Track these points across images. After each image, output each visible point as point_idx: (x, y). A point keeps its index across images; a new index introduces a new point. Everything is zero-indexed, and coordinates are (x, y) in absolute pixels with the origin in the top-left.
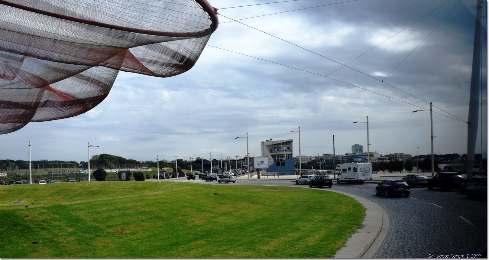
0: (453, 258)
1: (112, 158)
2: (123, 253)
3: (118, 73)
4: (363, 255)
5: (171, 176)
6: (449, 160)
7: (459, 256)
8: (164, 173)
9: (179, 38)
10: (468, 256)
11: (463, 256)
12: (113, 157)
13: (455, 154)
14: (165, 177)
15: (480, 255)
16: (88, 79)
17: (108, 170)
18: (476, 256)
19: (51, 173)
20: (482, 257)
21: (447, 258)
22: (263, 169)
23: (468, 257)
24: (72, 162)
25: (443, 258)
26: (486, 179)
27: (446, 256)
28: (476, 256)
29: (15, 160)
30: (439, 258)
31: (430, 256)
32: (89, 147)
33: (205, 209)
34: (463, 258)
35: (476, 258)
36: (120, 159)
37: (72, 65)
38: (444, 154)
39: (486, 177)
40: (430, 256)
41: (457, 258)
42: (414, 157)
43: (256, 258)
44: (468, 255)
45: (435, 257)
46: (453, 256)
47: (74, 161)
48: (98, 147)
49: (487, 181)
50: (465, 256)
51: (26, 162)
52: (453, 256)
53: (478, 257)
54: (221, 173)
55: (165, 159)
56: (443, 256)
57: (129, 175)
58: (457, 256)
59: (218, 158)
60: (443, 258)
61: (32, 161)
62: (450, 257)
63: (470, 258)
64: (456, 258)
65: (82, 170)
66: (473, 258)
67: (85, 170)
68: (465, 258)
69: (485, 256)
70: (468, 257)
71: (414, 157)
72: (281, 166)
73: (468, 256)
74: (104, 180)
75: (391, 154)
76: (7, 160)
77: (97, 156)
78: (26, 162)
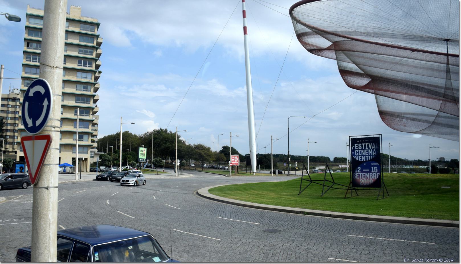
0: (432, 262)
1: (384, 156)
6: (33, 103)
7: (433, 260)
10: (441, 260)
11: (437, 260)
12: (385, 156)
15: (452, 260)
16: (128, 33)
20: (454, 262)
24: (343, 158)
32: (308, 142)
33: (410, 191)
34: (436, 262)
37: (453, 116)
41: (431, 262)
44: (441, 259)
45: (411, 261)
46: (427, 260)
48: (277, 139)
49: (459, 178)
51: (280, 155)
52: (427, 260)
53: (451, 262)
55: (406, 159)
58: (431, 260)
60: (417, 262)
63: (443, 262)
65: (405, 166)
67: (407, 166)
68: (439, 262)
69: (458, 261)
70: (441, 261)
72: (309, 156)
73: (441, 260)
74: (256, 170)
78: (280, 155)
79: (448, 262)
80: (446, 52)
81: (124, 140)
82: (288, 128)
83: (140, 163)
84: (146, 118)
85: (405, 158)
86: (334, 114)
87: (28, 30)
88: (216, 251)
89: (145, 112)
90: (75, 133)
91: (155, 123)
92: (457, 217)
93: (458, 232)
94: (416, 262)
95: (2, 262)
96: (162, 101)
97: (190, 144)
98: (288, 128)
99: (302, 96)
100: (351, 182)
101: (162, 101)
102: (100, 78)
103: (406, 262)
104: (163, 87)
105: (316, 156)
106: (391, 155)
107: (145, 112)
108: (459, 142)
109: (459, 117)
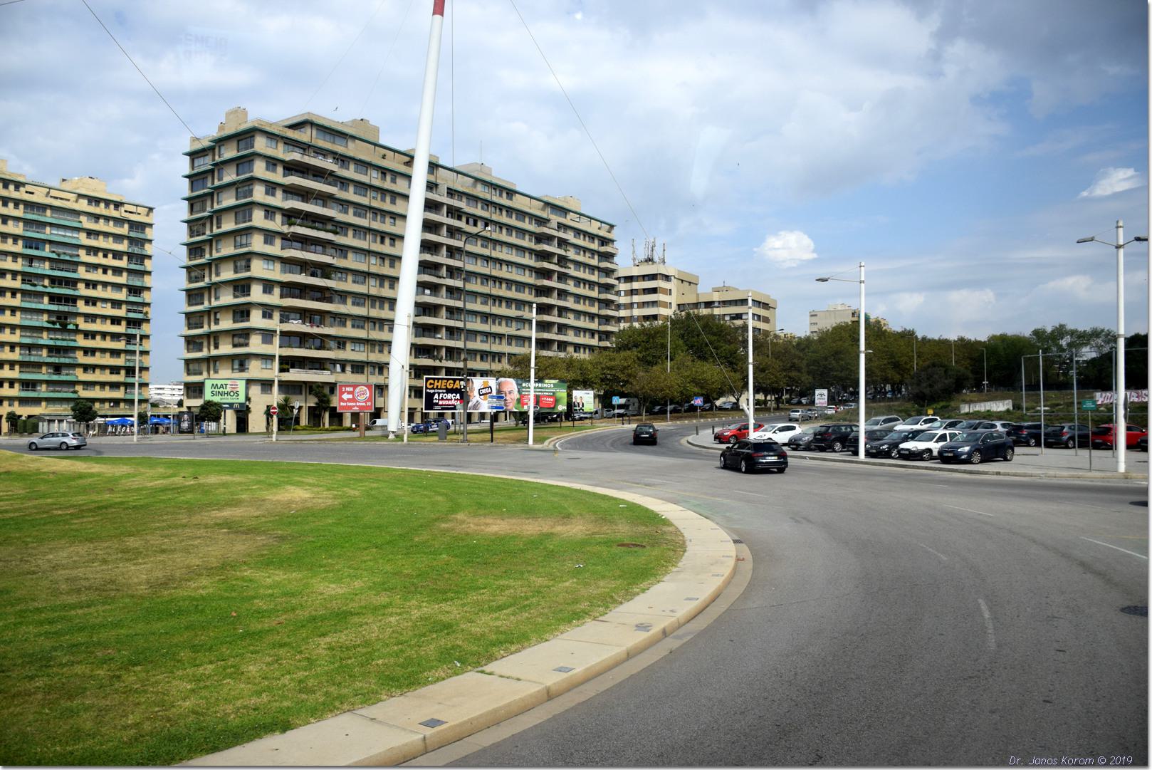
2: (516, 764)
4: (696, 616)
7: (1082, 761)
10: (1103, 760)
15: (1130, 759)
18: (1122, 761)
20: (1134, 764)
23: (1103, 763)
26: (1146, 434)
27: (1050, 761)
28: (1122, 761)
31: (1013, 759)
34: (1091, 764)
39: (1130, 432)
40: (1013, 759)
41: (1077, 765)
42: (920, 337)
43: (306, 239)
44: (1103, 757)
49: (1147, 350)
50: (1096, 761)
53: (1126, 765)
56: (1044, 761)
57: (126, 760)
62: (1059, 765)
63: (1107, 765)
64: (1073, 765)
66: (1115, 765)
68: (1095, 765)
71: (920, 337)
73: (1103, 760)
75: (905, 330)
79: (1121, 765)
80: (377, 148)
87: (267, 161)
90: (271, 357)
92: (1143, 438)
93: (1147, 516)
94: (1039, 766)
102: (755, 299)
103: (1015, 766)
105: (226, 751)
108: (1140, 620)
109: (1147, 443)
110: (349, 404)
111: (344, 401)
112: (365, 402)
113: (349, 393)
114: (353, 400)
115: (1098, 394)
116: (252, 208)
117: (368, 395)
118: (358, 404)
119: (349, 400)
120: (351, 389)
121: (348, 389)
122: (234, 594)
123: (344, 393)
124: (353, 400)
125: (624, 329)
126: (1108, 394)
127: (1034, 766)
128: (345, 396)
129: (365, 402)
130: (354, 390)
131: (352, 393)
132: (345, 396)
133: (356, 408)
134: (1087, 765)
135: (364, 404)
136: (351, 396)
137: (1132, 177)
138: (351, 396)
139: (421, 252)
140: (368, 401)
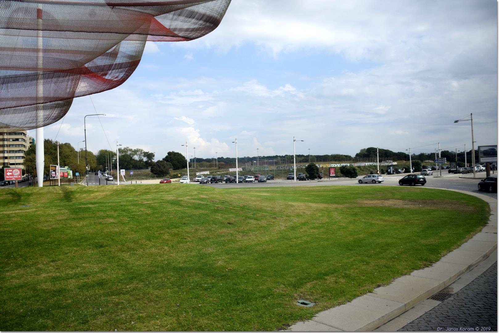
3: (145, 43)
5: (403, 171)
8: (391, 167)
9: (193, 4)
13: (222, 157)
14: (392, 173)
15: (489, 328)
17: (337, 165)
19: (279, 169)
21: (456, 331)
22: (17, 184)
23: (478, 330)
25: (452, 331)
29: (305, 155)
30: (448, 331)
34: (472, 331)
35: (485, 331)
36: (386, 152)
38: (231, 158)
41: (467, 331)
44: (478, 328)
46: (462, 329)
47: (347, 155)
53: (488, 331)
54: (454, 168)
59: (312, 155)
61: (296, 155)
62: (459, 331)
63: (480, 330)
64: (465, 331)
68: (475, 331)
70: (478, 330)
76: (398, 153)
77: (364, 149)
81: (46, 153)
82: (85, 130)
83: (76, 176)
84: (185, 125)
85: (159, 160)
86: (381, 109)
88: (161, 308)
89: (184, 118)
91: (195, 130)
95: (2, 331)
96: (201, 106)
97: (414, 154)
98: (85, 130)
99: (344, 92)
100: (16, 192)
101: (201, 106)
104: (200, 92)
106: (240, 157)
107: (184, 118)
110: (10, 177)
111: (8, 176)
112: (18, 176)
113: (10, 172)
114: (12, 175)
115: (230, 169)
116: (79, 79)
117: (19, 173)
118: (15, 177)
119: (10, 175)
120: (11, 171)
121: (9, 171)
122: (30, 274)
123: (7, 172)
124: (12, 175)
125: (245, 163)
126: (235, 169)
127: (448, 331)
128: (8, 174)
129: (18, 176)
130: (13, 171)
131: (12, 172)
132: (8, 174)
133: (14, 179)
134: (471, 331)
135: (17, 177)
136: (11, 174)
137: (86, 86)
138: (11, 174)
139: (496, 146)
140: (19, 175)
